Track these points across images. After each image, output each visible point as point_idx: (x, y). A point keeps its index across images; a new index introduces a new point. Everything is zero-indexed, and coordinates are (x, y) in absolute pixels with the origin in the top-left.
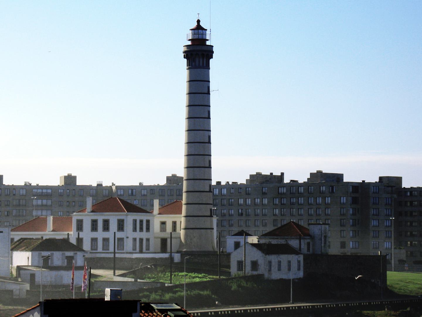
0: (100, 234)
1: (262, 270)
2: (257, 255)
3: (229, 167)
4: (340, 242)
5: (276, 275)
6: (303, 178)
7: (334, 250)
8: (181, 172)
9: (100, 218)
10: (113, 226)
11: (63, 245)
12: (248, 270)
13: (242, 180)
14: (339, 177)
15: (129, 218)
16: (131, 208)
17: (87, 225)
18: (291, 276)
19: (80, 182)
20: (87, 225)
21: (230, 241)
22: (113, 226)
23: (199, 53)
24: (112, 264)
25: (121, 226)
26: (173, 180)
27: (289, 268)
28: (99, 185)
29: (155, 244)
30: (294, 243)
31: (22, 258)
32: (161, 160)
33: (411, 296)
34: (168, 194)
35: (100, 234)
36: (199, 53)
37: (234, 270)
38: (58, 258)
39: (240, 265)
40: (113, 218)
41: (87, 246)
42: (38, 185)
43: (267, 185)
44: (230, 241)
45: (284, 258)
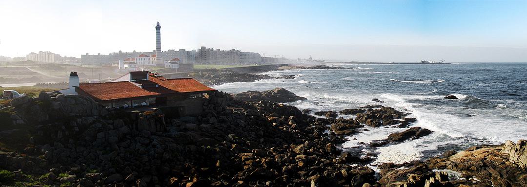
0: (141, 61)
1: (171, 67)
2: (170, 64)
3: (164, 48)
4: (185, 61)
5: (173, 68)
6: (178, 50)
7: (184, 63)
8: (155, 49)
9: (140, 58)
10: (143, 59)
11: (134, 63)
12: (168, 67)
13: (167, 51)
14: (184, 50)
15: (146, 58)
16: (146, 56)
17: (138, 59)
18: (176, 68)
19: (89, 54)
20: (138, 59)
21: (165, 62)
22: (143, 59)
23: (158, 27)
24: (143, 66)
25: (144, 60)
26: (154, 51)
27: (176, 66)
28: (110, 54)
29: (151, 62)
30: (177, 62)
31: (126, 66)
32: (151, 47)
33: (288, 102)
34: (153, 54)
35: (141, 61)
36: (158, 27)
37: (166, 67)
38: (133, 65)
39: (167, 66)
40: (143, 58)
41: (138, 63)
42: (233, 50)
43: (171, 52)
44: (165, 62)
45: (175, 64)
